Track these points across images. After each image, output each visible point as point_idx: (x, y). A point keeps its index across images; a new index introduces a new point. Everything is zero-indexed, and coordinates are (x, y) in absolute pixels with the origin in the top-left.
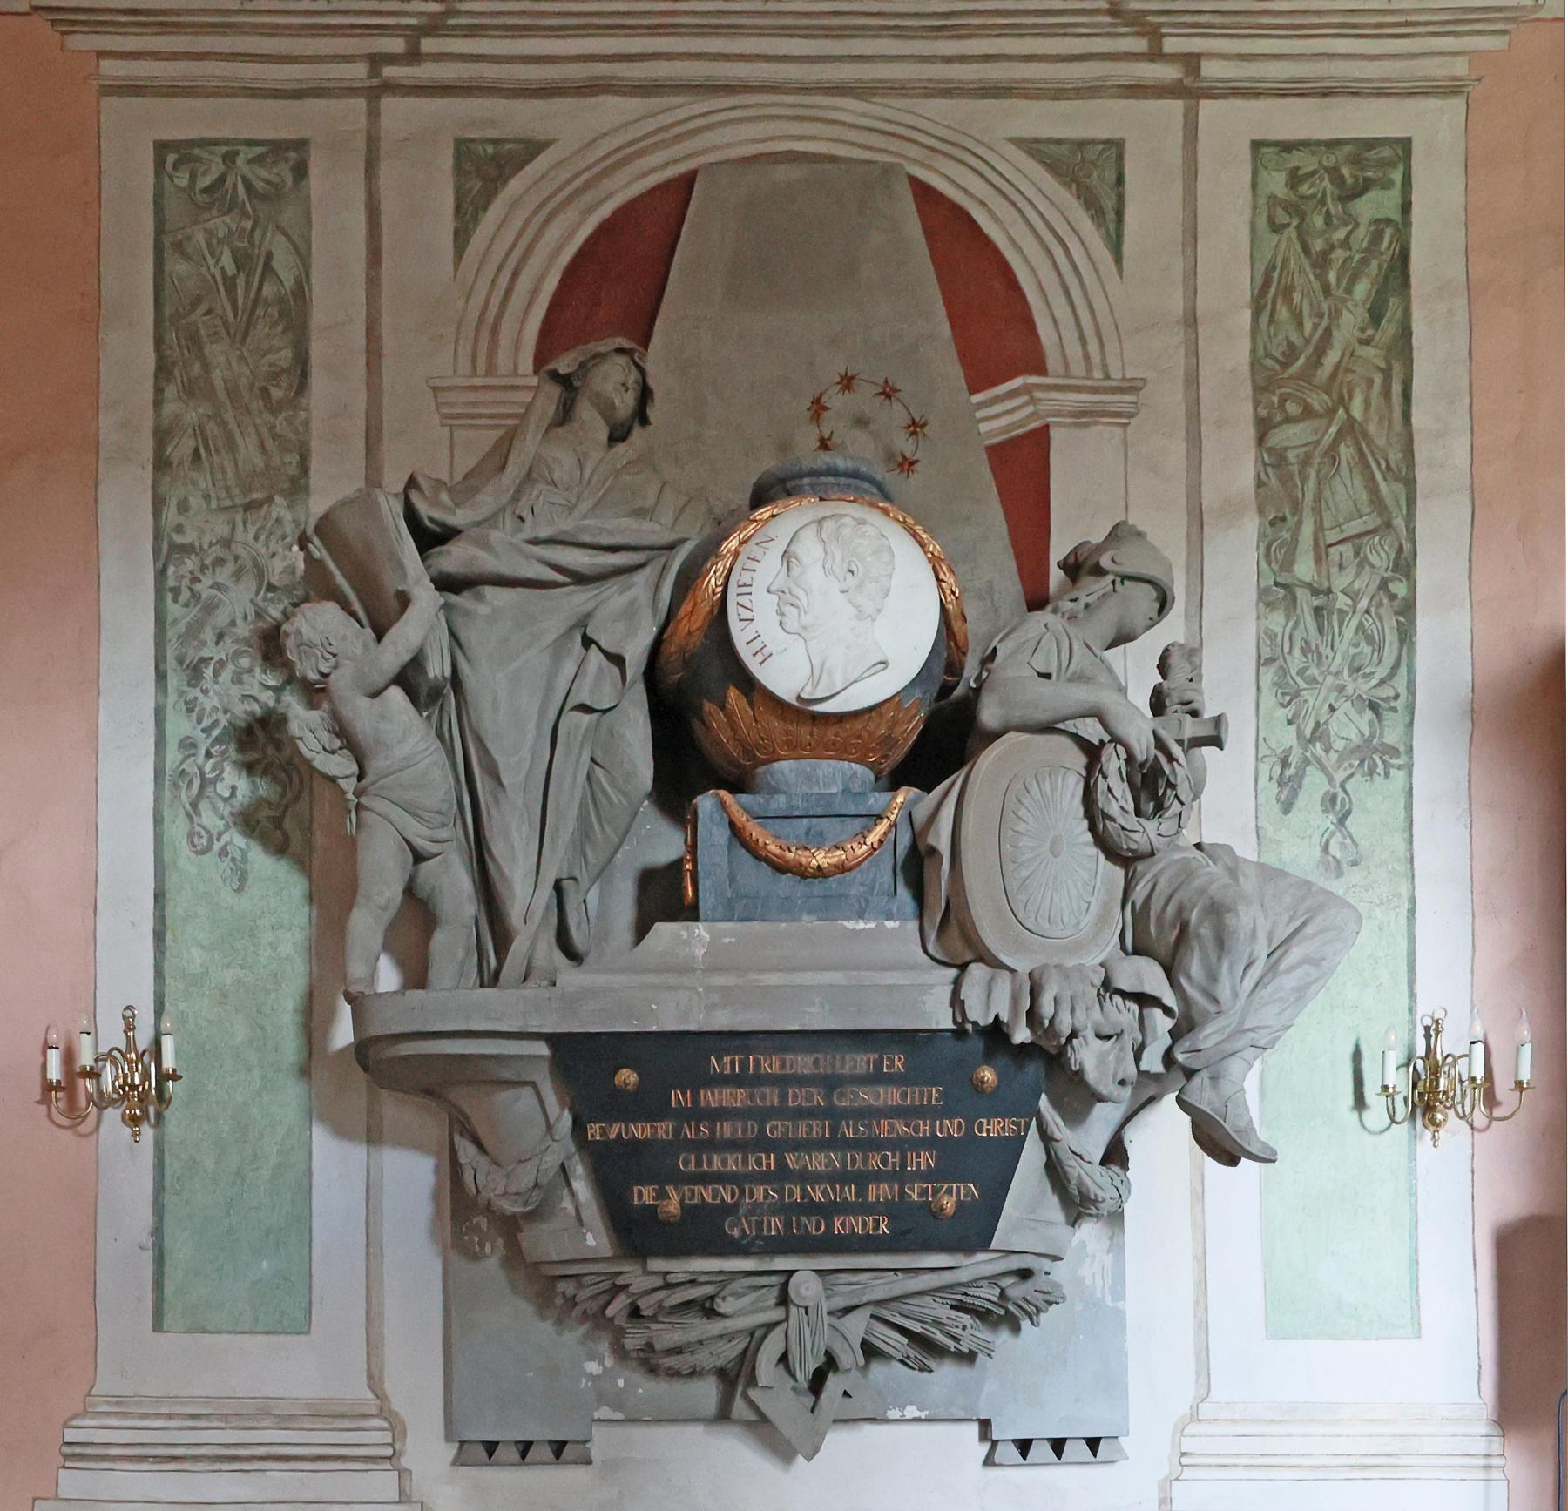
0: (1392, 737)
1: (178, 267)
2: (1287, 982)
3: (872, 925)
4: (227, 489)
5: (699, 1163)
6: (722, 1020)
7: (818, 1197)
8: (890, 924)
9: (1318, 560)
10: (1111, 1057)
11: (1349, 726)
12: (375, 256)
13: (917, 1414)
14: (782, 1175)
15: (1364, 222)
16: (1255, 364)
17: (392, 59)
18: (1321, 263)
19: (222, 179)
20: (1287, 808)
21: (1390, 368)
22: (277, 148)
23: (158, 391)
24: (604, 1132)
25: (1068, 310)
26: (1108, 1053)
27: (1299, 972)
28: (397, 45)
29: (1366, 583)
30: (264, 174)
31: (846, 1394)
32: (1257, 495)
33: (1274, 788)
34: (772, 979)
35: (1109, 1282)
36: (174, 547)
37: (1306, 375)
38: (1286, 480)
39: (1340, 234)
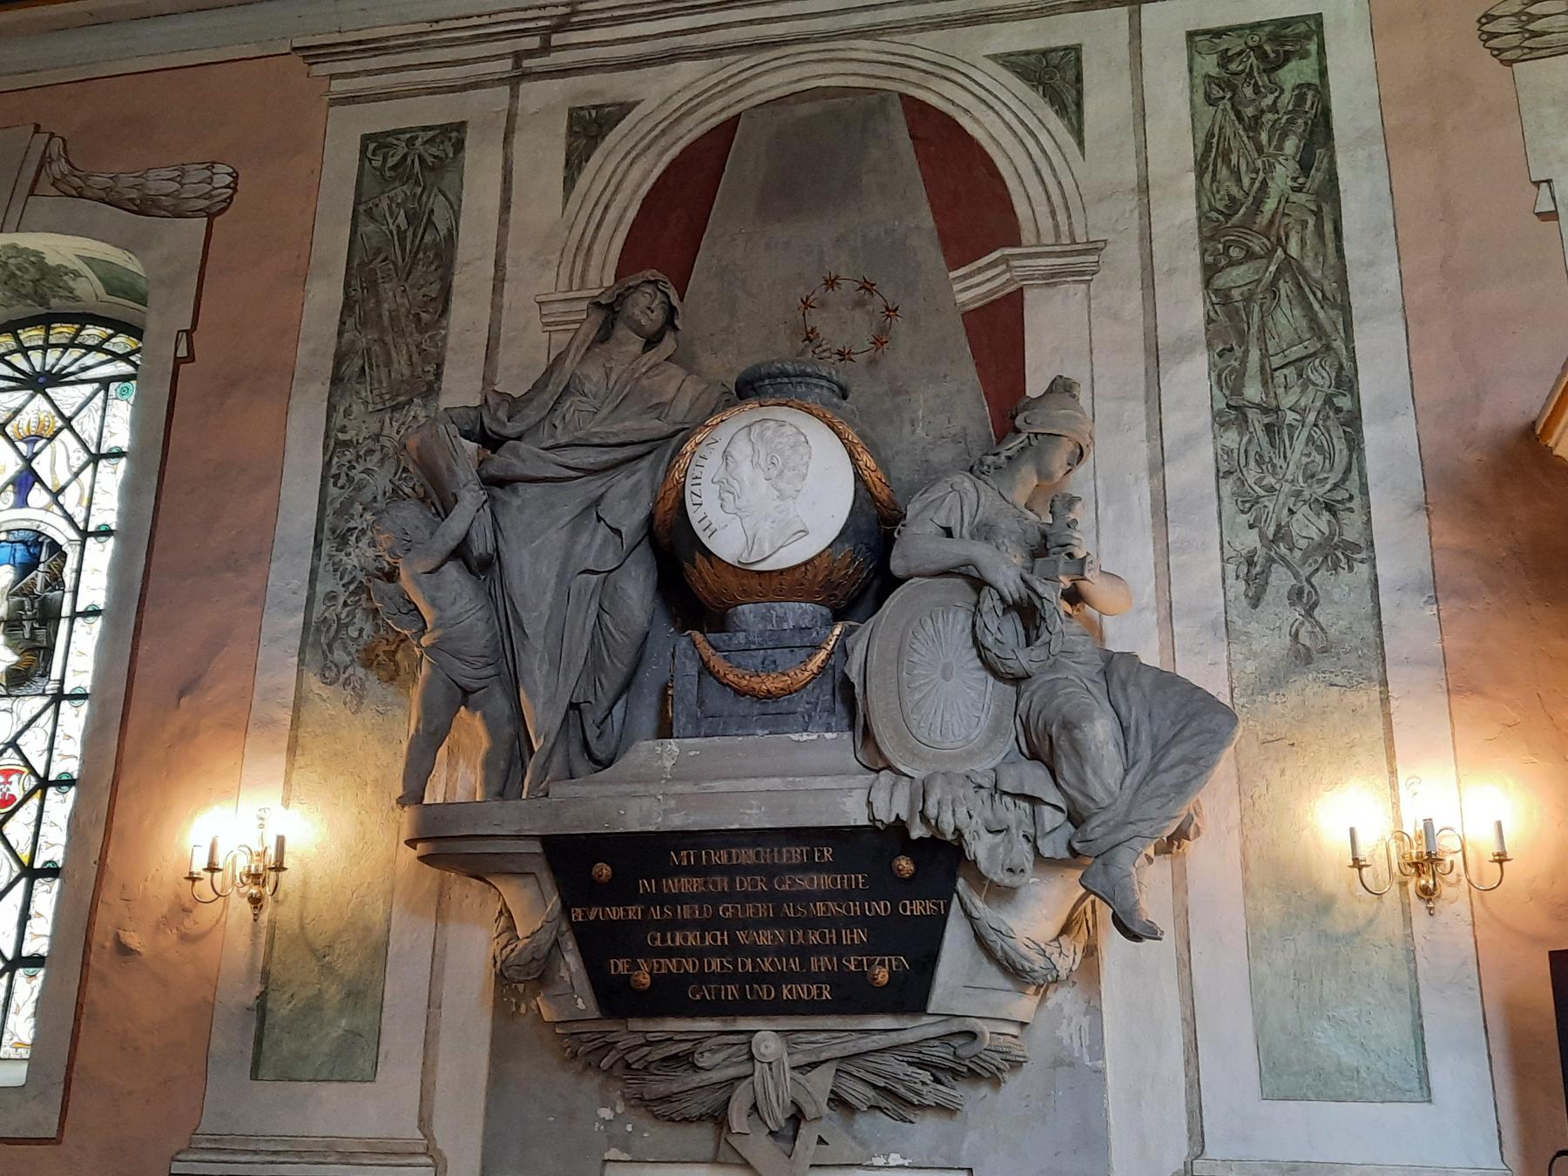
0: (1351, 535)
1: (368, 228)
2: (1169, 779)
3: (815, 736)
4: (381, 396)
5: (664, 940)
6: (677, 822)
7: (767, 967)
8: (829, 736)
9: (1265, 384)
10: (1001, 849)
11: (1309, 527)
12: (506, 206)
13: (901, 1162)
14: (734, 948)
15: (1288, 87)
16: (1202, 218)
17: (530, 53)
18: (1253, 126)
19: (405, 157)
20: (1255, 602)
21: (1320, 208)
22: (445, 129)
23: (342, 322)
24: (585, 915)
25: (1041, 189)
26: (997, 845)
27: (1177, 771)
28: (534, 42)
29: (1312, 399)
30: (434, 151)
31: (821, 1141)
32: (1207, 330)
33: (1242, 585)
34: (722, 786)
35: (1086, 1042)
36: (339, 443)
37: (1246, 225)
38: (1233, 315)
39: (1269, 100)
